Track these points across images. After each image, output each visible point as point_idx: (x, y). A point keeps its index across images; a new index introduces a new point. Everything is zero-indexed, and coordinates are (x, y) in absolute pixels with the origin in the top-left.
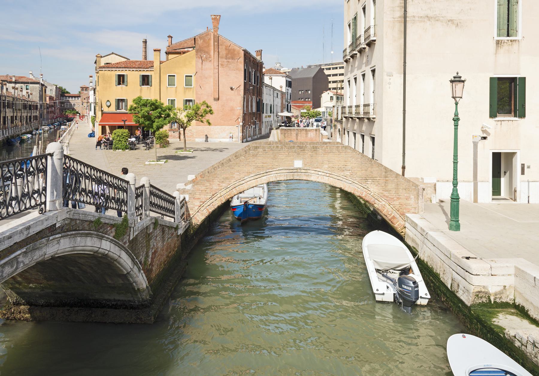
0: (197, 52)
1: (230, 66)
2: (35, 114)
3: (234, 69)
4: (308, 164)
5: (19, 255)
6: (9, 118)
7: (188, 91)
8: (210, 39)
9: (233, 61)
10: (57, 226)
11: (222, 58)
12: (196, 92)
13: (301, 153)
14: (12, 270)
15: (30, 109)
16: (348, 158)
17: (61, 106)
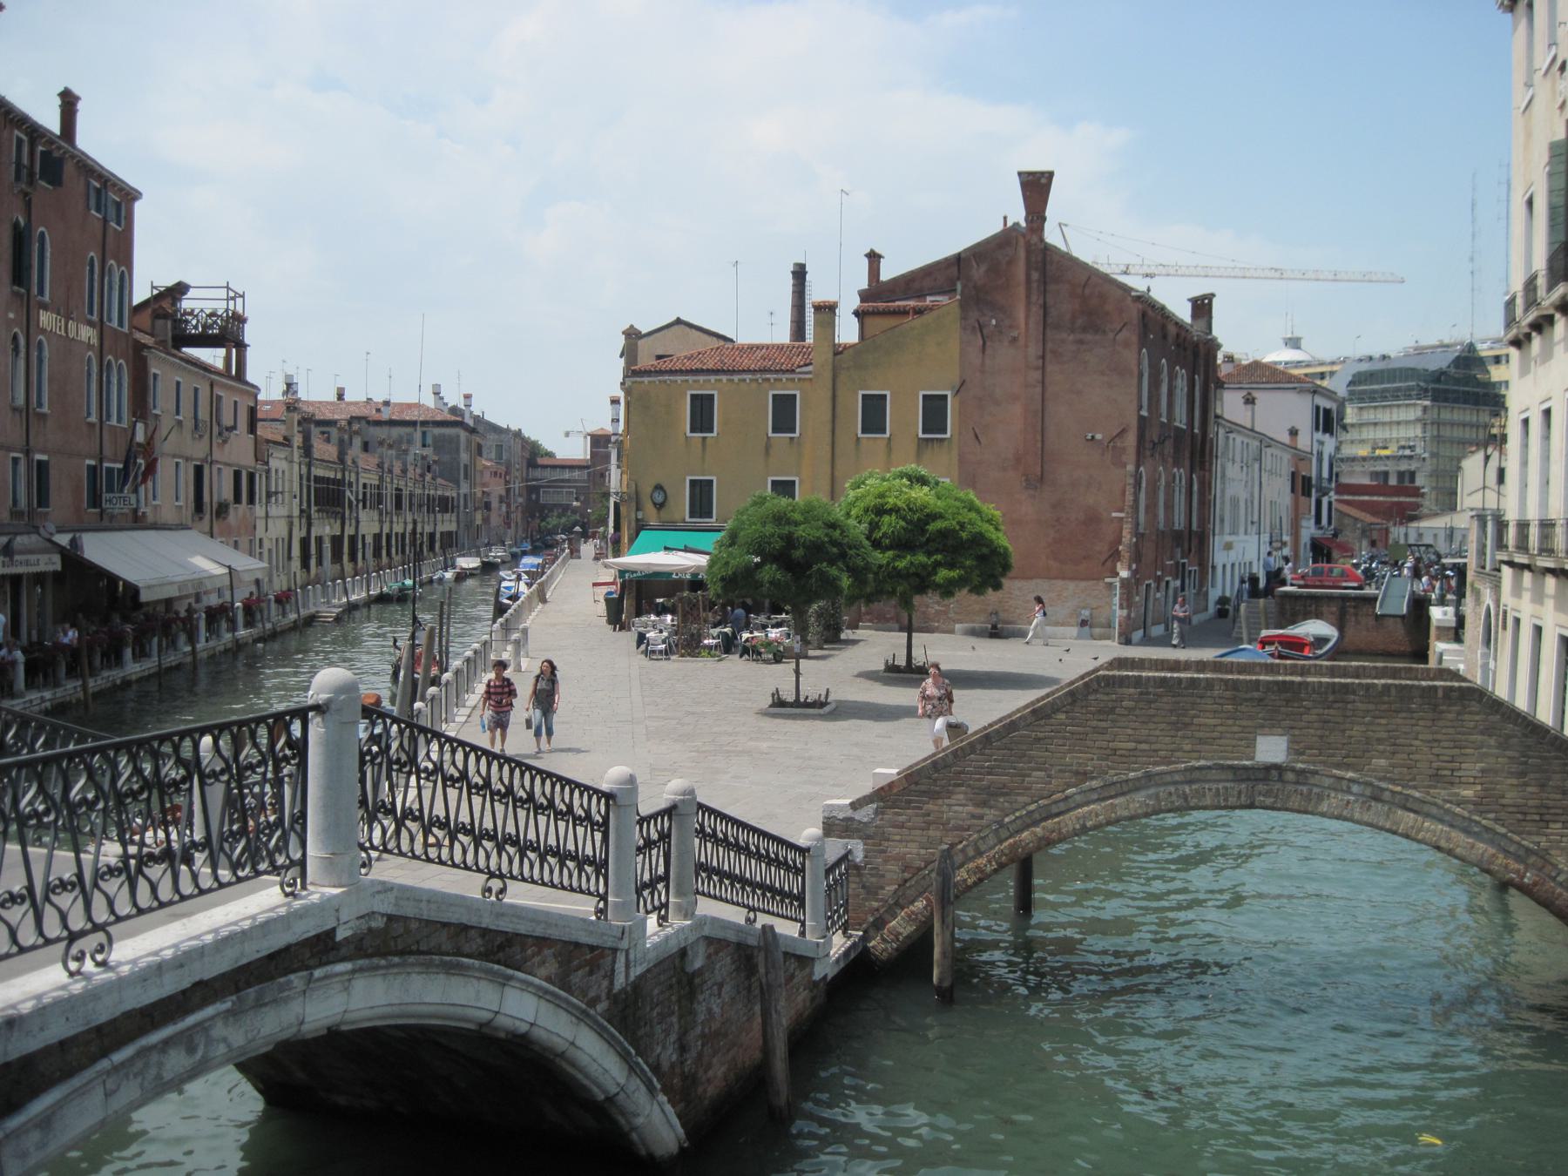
0: (964, 305)
5: (212, 1018)
6: (369, 540)
8: (1010, 263)
10: (341, 935)
14: (192, 1061)
17: (529, 499)
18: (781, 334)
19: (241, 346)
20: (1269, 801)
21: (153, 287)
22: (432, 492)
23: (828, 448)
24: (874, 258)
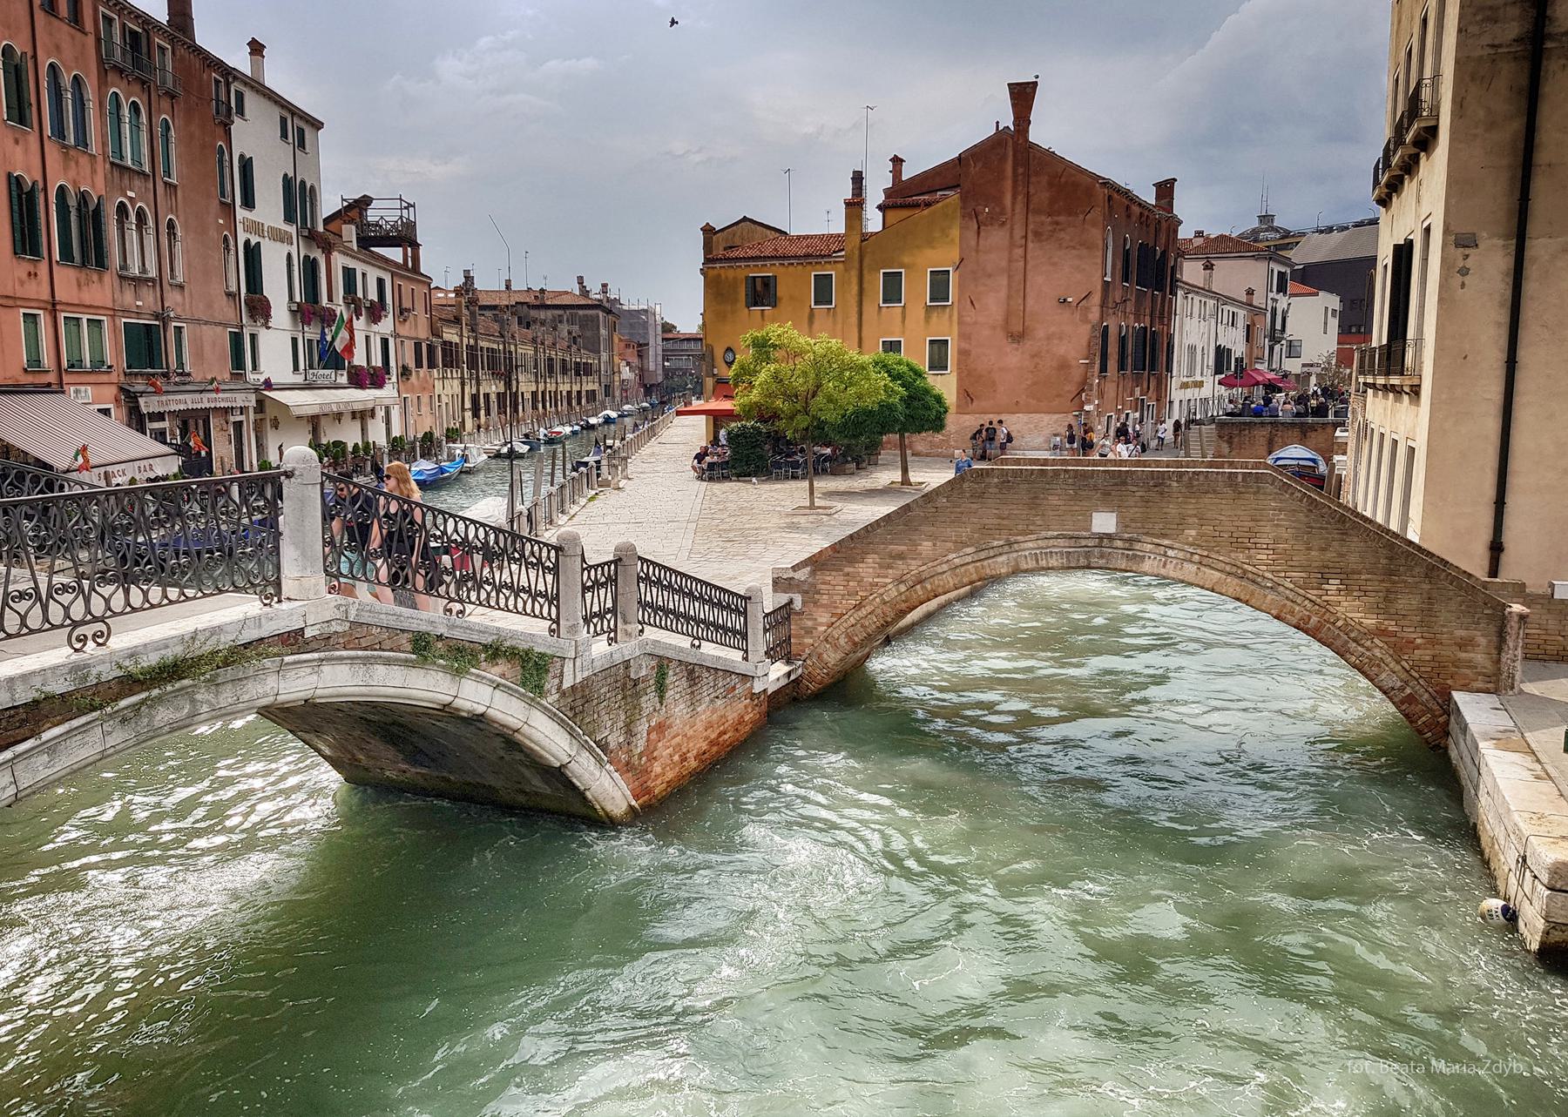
1: (1062, 235)
2: (590, 387)
3: (1071, 244)
4: (1133, 525)
6: (528, 396)
7: (936, 314)
9: (1070, 218)
10: (309, 633)
11: (1038, 212)
12: (960, 316)
13: (1113, 493)
15: (578, 374)
16: (1264, 509)
18: (838, 226)
19: (415, 245)
20: (1102, 562)
21: (343, 200)
22: (578, 360)
23: (1493, 426)
24: (897, 161)
